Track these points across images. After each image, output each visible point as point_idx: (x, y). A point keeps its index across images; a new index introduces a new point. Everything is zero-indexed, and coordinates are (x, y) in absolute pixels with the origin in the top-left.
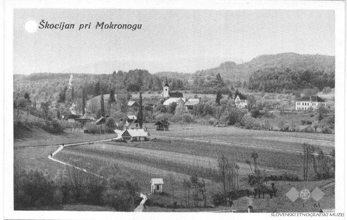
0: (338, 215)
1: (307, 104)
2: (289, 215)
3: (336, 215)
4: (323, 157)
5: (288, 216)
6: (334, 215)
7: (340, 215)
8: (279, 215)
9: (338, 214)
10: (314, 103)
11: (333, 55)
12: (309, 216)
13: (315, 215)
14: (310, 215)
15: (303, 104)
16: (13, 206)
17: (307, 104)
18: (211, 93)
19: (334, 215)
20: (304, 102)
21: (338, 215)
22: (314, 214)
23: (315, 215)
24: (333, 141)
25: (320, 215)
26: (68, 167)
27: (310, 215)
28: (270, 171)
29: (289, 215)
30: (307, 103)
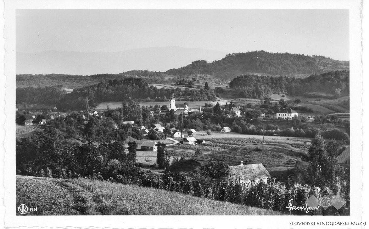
0: (360, 224)
1: (285, 115)
2: (308, 224)
3: (357, 224)
4: (71, 214)
5: (307, 225)
6: (356, 224)
7: (362, 224)
8: (298, 223)
9: (360, 223)
10: (290, 115)
11: (347, 60)
12: (330, 223)
13: (336, 224)
14: (330, 224)
15: (282, 115)
16: (15, 172)
17: (285, 115)
18: (188, 149)
19: (356, 224)
20: (283, 114)
21: (360, 224)
22: (335, 223)
23: (336, 224)
24: (349, 119)
25: (341, 224)
26: (311, 91)
27: (330, 224)
28: (292, 158)
29: (308, 224)
30: (285, 114)
